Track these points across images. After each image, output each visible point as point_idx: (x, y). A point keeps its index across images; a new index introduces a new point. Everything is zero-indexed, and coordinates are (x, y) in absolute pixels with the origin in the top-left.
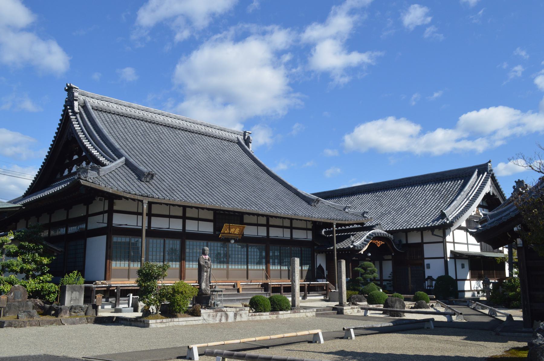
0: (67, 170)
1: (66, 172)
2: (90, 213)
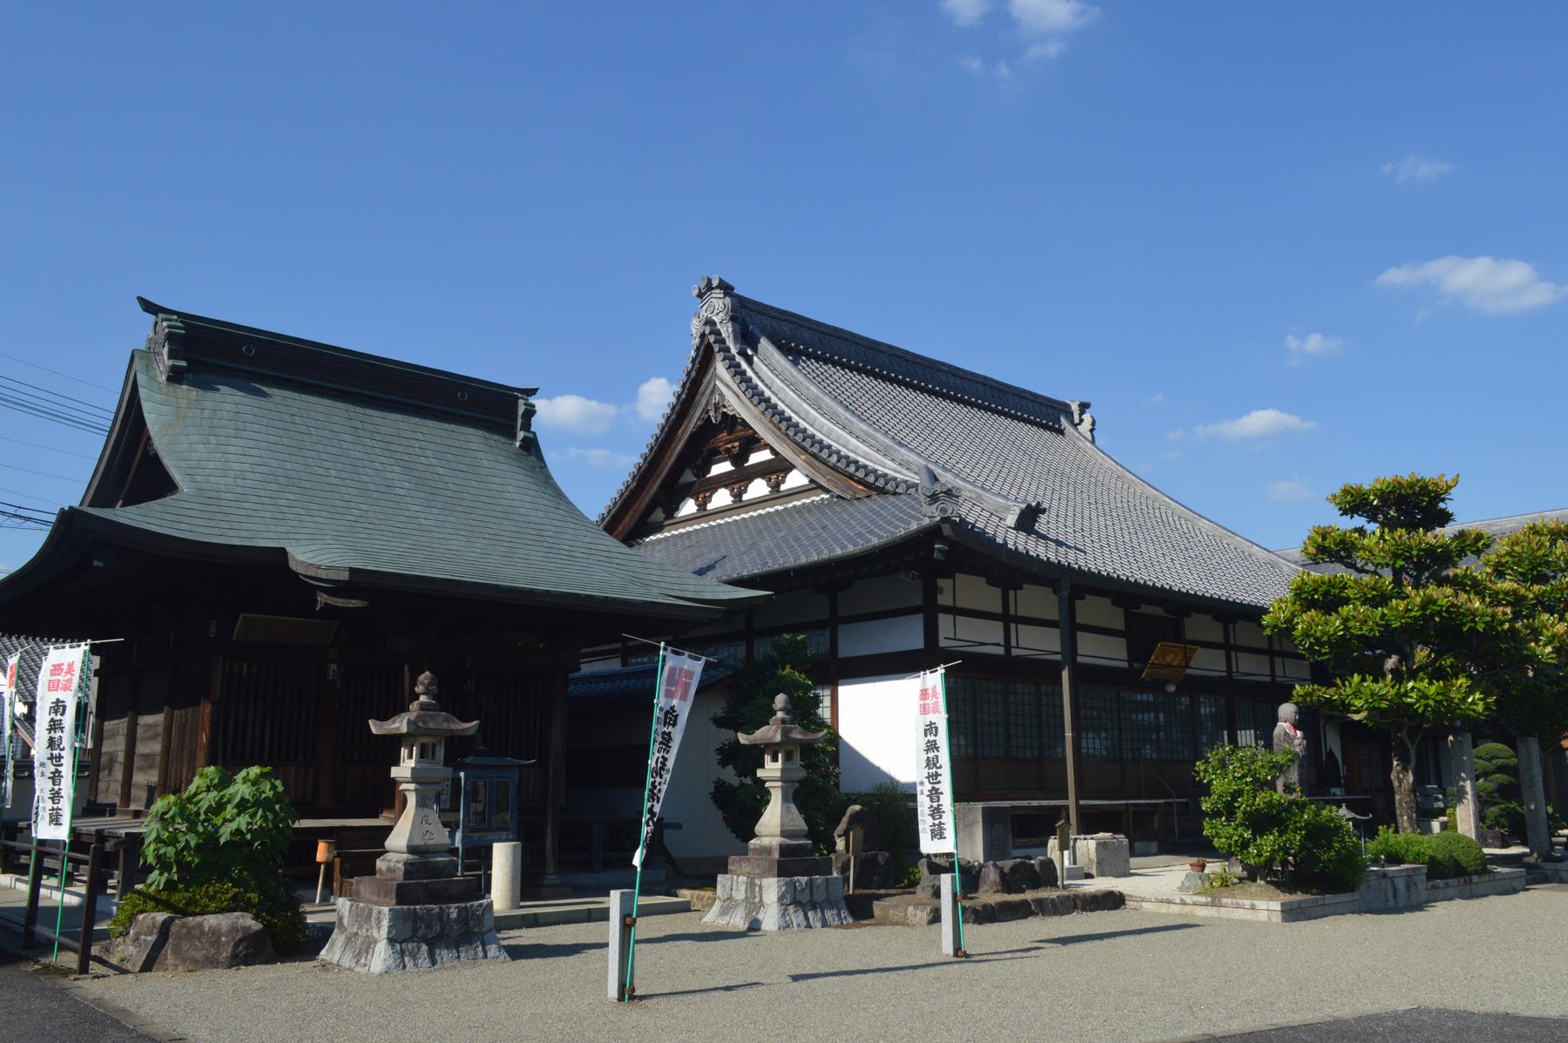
1: (689, 507)
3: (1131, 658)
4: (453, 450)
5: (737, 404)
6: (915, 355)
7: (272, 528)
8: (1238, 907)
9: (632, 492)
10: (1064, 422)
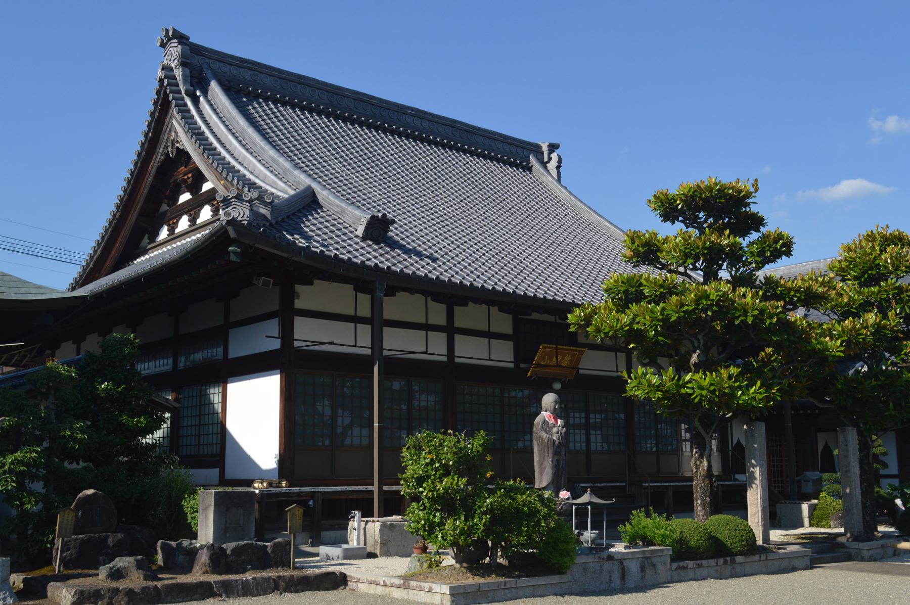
0: (165, 228)
1: (164, 234)
2: (232, 319)
3: (517, 360)
5: (187, 143)
6: (381, 100)
8: (421, 589)
9: (118, 221)
10: (532, 159)
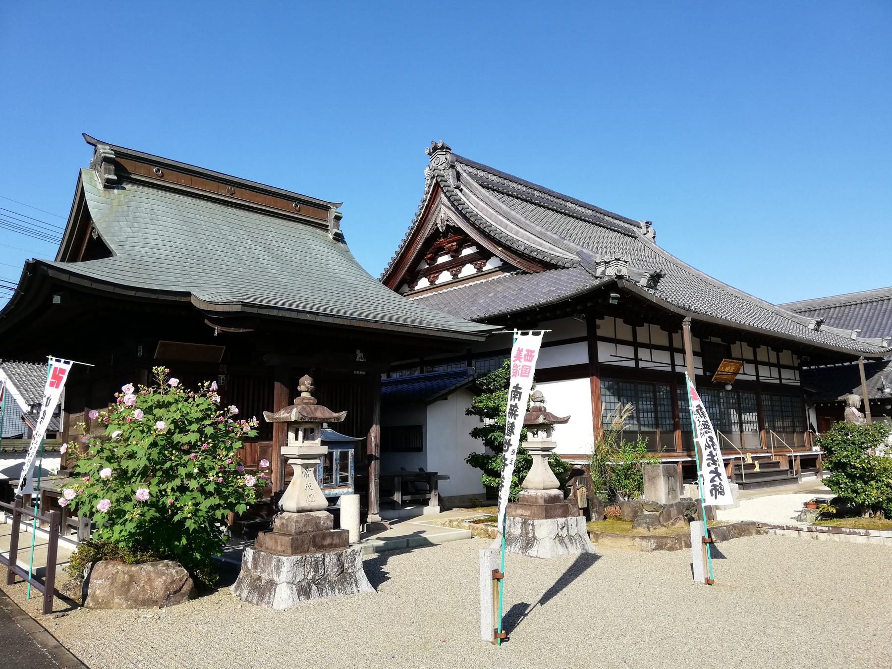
1: (423, 283)
4: (293, 239)
7: (180, 279)
